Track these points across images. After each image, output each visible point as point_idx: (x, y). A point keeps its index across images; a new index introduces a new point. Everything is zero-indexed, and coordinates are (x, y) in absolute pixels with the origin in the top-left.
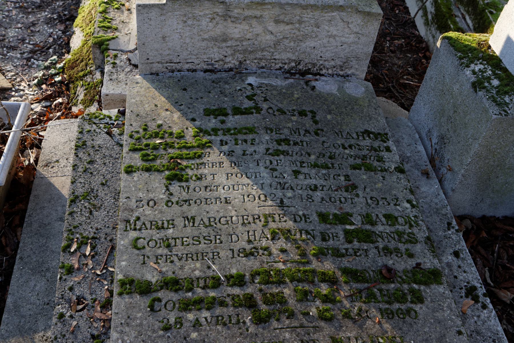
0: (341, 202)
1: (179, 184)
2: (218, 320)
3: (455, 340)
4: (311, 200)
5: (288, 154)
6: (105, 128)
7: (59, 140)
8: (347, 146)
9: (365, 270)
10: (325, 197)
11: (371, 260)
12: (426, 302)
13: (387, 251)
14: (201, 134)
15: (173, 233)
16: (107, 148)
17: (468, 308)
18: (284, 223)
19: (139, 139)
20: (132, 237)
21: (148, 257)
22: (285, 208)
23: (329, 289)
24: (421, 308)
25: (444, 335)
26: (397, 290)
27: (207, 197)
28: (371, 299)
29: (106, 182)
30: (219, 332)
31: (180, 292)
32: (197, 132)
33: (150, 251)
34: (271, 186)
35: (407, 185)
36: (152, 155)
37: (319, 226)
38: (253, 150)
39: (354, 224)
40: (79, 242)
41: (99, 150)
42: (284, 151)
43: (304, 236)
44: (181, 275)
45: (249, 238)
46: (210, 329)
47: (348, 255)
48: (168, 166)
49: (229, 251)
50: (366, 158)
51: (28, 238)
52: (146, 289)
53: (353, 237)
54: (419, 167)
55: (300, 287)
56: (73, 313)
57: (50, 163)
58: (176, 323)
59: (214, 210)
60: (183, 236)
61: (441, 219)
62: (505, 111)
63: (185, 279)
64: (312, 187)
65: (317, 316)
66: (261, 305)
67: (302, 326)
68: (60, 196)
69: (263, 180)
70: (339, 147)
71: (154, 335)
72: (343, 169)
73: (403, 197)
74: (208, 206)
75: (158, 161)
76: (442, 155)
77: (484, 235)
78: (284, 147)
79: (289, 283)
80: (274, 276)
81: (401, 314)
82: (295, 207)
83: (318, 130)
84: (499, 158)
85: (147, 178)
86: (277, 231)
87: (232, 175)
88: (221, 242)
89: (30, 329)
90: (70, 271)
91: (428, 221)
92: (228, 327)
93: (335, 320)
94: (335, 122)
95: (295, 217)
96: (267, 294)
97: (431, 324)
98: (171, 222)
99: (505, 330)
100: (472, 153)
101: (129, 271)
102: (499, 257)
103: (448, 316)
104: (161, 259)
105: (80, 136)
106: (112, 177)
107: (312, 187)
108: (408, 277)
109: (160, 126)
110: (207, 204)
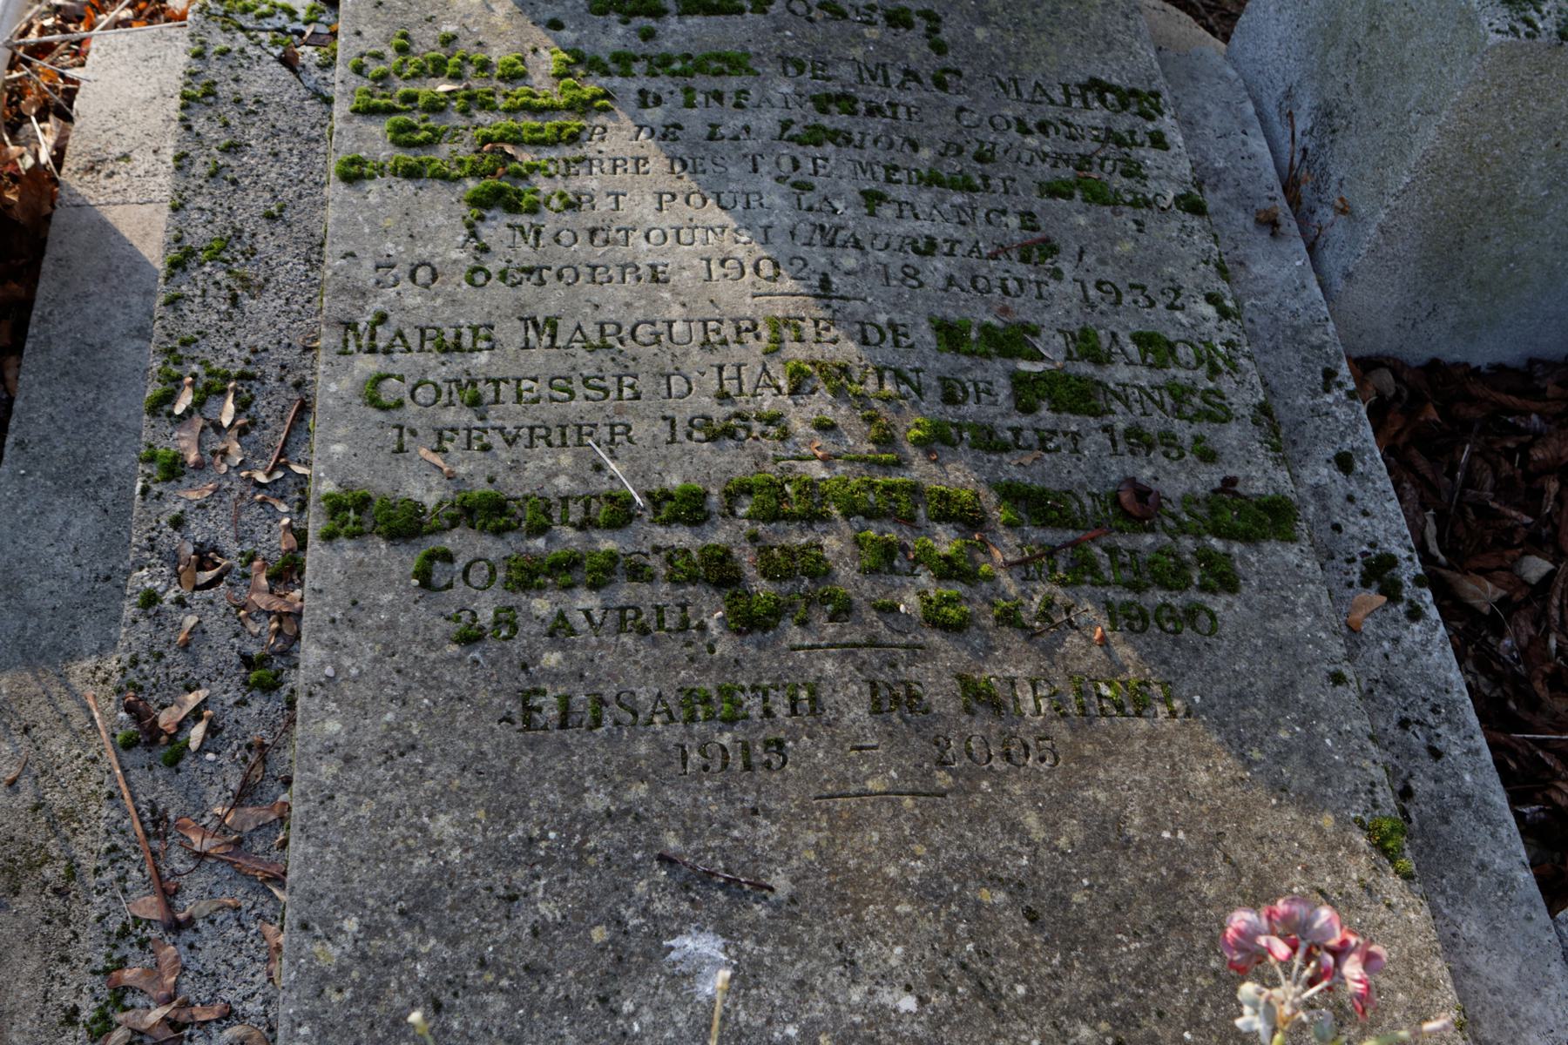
0: (1005, 291)
1: (508, 219)
2: (623, 620)
3: (1323, 698)
4: (915, 283)
5: (849, 141)
6: (275, 44)
7: (129, 92)
8: (1031, 124)
9: (1068, 492)
10: (957, 275)
11: (1088, 463)
12: (1244, 590)
13: (1138, 440)
14: (580, 71)
15: (489, 364)
16: (283, 107)
17: (1368, 615)
18: (831, 347)
19: (383, 77)
20: (362, 371)
21: (413, 433)
22: (835, 303)
23: (958, 542)
24: (1229, 606)
25: (1292, 684)
26: (1160, 552)
27: (594, 262)
28: (1084, 573)
29: (281, 209)
30: (625, 653)
31: (511, 537)
32: (568, 64)
33: (420, 415)
34: (793, 234)
35: (1211, 249)
36: (426, 129)
37: (936, 359)
38: (740, 124)
39: (1043, 358)
40: (200, 386)
41: (255, 113)
42: (836, 132)
43: (889, 387)
44: (513, 486)
45: (721, 385)
46: (601, 644)
47: (1019, 447)
48: (473, 162)
49: (661, 422)
50: (1090, 163)
51: (40, 384)
52: (405, 525)
53: (1038, 396)
54: (1249, 202)
55: (872, 534)
56: (185, 592)
57: (103, 161)
58: (497, 623)
59: (617, 300)
60: (519, 375)
61: (1304, 359)
62: (1530, 23)
63: (526, 498)
64: (921, 244)
65: (918, 615)
66: (755, 580)
67: (873, 643)
68: (138, 264)
69: (768, 215)
70: (1009, 127)
71: (433, 656)
72: (1016, 194)
73: (1197, 286)
74: (597, 287)
75: (445, 149)
76: (1324, 166)
77: (1432, 414)
78: (836, 120)
79: (840, 519)
80: (794, 497)
81: (1169, 619)
82: (864, 300)
83: (946, 71)
84: (1497, 176)
85: (409, 199)
86: (808, 367)
87: (674, 197)
88: (637, 397)
89: (56, 648)
90: (174, 469)
91: (1266, 365)
92: (654, 638)
93: (973, 628)
94: (998, 51)
95: (863, 331)
96: (772, 548)
97: (1256, 650)
98: (482, 332)
99: (1468, 686)
100: (1415, 155)
101: (353, 472)
102: (1470, 482)
103: (1307, 629)
104: (452, 440)
105: (197, 66)
106: (300, 196)
107: (921, 244)
108: (1195, 516)
109: (448, 40)
110: (594, 281)
